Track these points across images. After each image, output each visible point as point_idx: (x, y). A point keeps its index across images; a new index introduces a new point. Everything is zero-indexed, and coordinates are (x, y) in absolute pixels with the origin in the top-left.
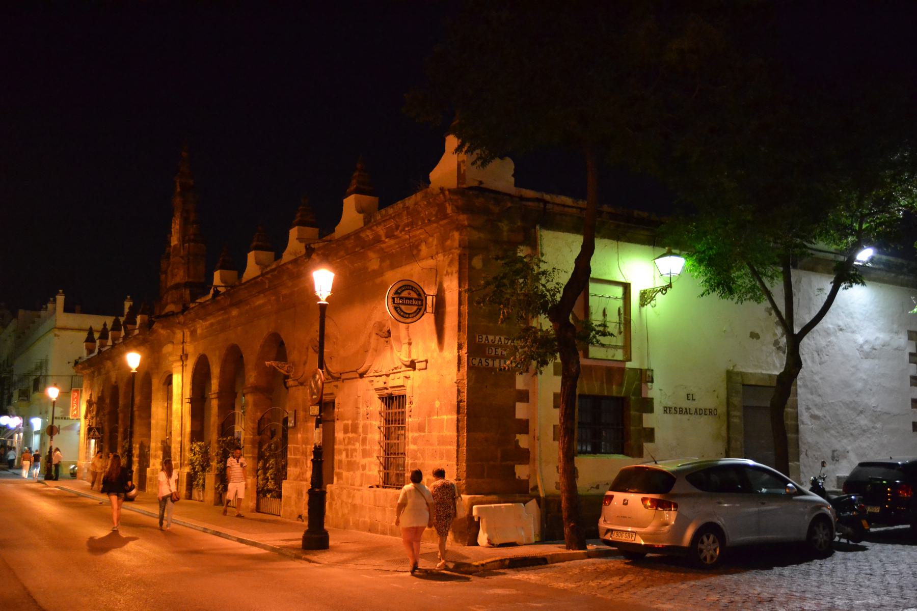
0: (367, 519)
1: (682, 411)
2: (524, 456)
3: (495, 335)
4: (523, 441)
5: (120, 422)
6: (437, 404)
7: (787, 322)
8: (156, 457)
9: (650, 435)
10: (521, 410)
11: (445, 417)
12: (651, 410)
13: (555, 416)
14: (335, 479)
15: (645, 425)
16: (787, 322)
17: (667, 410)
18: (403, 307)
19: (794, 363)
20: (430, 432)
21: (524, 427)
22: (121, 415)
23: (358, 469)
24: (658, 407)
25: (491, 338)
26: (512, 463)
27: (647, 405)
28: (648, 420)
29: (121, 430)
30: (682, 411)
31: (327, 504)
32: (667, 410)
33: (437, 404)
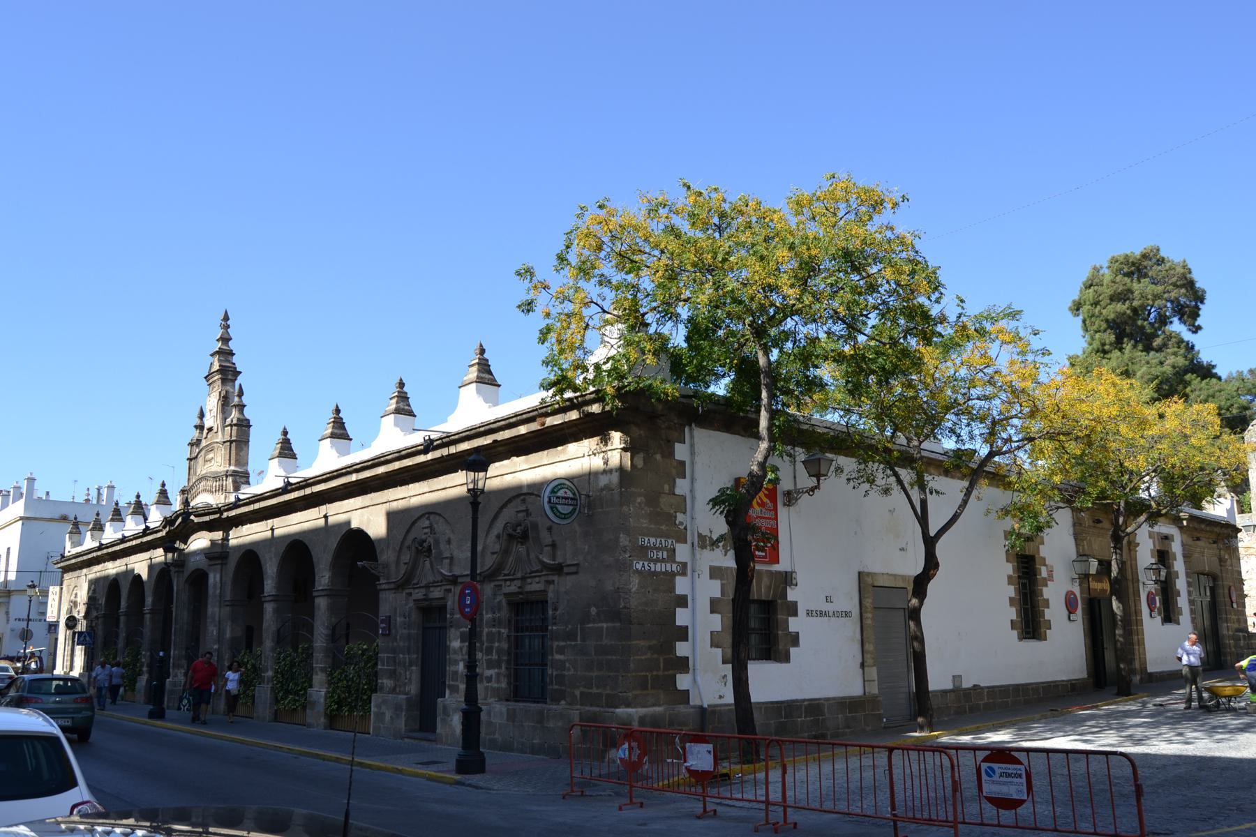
0: (497, 736)
1: (822, 614)
2: (683, 665)
3: (656, 536)
4: (682, 649)
5: (122, 625)
6: (593, 610)
7: (923, 519)
8: (454, 689)
9: (795, 640)
10: (682, 617)
11: (605, 625)
12: (795, 614)
13: (716, 622)
14: (447, 692)
15: (678, 623)
16: (923, 519)
17: (809, 613)
18: (559, 507)
19: (931, 564)
20: (583, 640)
21: (683, 634)
22: (122, 619)
23: (481, 681)
24: (801, 610)
25: (652, 540)
26: (671, 672)
27: (793, 609)
28: (794, 624)
29: (122, 635)
30: (822, 614)
31: (438, 719)
32: (809, 613)
33: (593, 610)
